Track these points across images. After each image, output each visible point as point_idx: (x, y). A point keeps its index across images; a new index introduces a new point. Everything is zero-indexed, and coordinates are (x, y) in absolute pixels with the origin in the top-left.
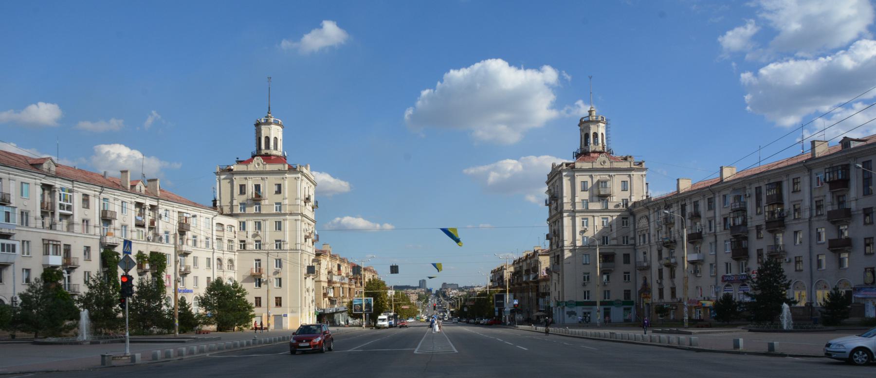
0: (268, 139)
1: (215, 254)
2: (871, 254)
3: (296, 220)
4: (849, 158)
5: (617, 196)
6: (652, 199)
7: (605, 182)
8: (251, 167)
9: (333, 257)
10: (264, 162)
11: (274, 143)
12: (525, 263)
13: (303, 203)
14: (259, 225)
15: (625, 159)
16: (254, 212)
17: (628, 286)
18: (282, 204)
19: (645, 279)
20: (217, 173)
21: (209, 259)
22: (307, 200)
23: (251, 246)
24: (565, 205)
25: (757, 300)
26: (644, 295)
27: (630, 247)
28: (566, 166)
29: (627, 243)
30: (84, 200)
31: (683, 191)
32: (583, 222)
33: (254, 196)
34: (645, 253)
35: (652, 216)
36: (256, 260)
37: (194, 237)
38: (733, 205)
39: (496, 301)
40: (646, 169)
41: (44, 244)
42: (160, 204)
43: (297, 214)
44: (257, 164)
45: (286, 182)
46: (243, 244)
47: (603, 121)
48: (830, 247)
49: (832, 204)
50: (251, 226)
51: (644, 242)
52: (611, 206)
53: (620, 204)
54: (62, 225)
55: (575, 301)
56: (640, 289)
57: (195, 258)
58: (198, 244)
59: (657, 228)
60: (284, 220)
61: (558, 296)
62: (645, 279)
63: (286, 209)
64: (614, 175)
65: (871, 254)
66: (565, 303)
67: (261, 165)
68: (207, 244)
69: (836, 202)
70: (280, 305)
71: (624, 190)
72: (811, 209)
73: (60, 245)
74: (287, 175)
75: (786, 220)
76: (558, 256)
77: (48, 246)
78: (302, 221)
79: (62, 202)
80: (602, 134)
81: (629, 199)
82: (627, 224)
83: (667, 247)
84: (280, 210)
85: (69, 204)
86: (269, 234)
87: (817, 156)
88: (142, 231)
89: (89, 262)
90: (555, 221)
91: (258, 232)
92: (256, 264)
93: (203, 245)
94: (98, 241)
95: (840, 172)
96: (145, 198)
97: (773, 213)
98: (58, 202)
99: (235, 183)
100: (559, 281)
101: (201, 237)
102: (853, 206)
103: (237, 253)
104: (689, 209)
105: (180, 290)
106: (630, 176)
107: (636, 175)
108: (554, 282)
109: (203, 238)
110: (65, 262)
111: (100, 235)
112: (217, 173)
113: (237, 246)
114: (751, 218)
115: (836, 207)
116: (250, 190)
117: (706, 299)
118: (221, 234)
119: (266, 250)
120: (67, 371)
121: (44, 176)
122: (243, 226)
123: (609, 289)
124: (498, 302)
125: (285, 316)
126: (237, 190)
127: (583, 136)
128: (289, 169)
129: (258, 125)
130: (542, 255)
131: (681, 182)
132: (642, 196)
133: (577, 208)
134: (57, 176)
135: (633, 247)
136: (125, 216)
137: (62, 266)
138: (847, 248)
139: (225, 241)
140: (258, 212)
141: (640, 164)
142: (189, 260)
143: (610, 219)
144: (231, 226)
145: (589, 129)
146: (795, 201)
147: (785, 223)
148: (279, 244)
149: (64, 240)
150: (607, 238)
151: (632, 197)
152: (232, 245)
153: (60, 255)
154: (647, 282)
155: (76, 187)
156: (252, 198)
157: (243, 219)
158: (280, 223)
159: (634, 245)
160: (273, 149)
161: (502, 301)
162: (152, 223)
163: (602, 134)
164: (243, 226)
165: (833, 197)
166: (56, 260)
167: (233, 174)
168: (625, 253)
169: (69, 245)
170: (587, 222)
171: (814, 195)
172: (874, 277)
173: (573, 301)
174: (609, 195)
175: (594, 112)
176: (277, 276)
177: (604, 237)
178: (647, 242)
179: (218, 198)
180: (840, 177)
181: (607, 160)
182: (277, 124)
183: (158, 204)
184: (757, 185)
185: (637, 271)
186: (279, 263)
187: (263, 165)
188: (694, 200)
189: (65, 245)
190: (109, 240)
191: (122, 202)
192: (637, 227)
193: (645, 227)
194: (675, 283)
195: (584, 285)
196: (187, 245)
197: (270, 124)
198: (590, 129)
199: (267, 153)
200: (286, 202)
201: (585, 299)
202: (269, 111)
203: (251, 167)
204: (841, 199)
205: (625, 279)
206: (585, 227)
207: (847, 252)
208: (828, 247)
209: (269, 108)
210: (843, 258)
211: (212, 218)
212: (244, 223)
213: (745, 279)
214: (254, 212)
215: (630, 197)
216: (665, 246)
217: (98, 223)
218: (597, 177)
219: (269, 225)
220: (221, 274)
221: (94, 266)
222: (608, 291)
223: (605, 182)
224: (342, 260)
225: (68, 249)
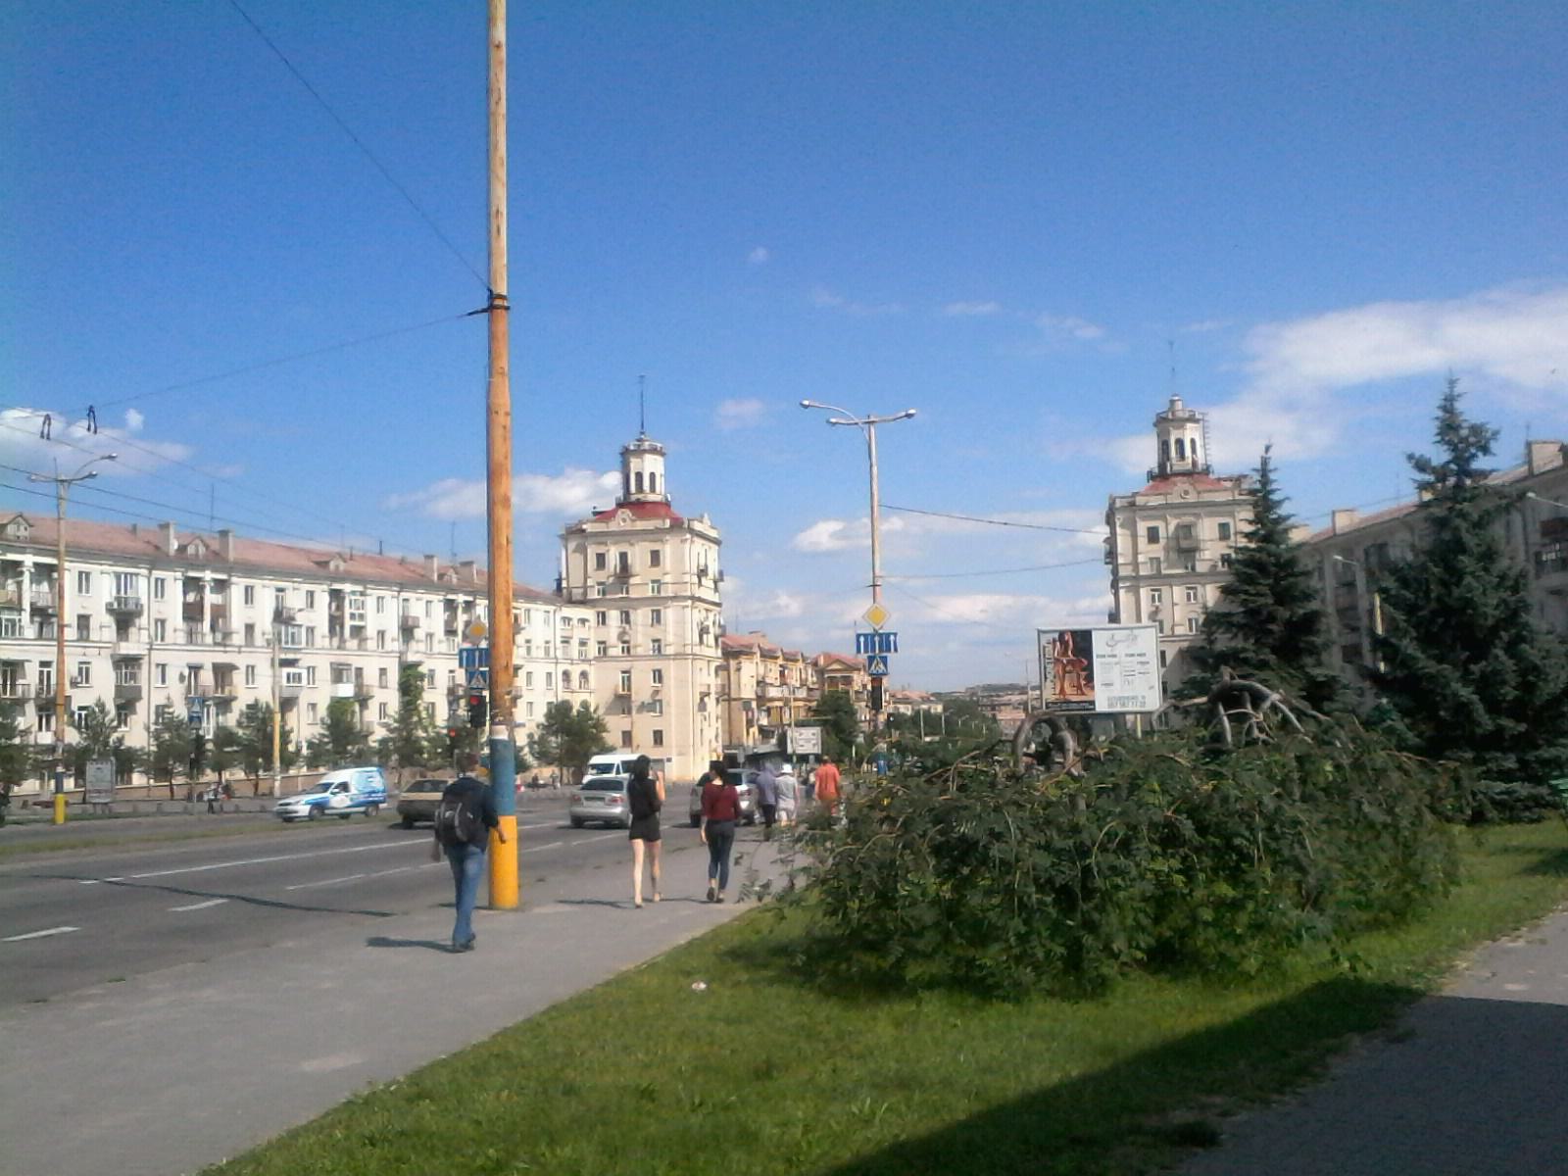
6: (604, 734)
8: (614, 526)
9: (768, 655)
13: (695, 579)
14: (626, 618)
22: (702, 573)
32: (1153, 596)
37: (528, 641)
43: (686, 598)
44: (624, 521)
50: (614, 616)
52: (1201, 567)
54: (352, 644)
57: (529, 674)
58: (534, 652)
68: (547, 651)
70: (661, 743)
77: (338, 673)
78: (692, 608)
79: (353, 611)
84: (659, 592)
85: (361, 611)
87: (1536, 472)
93: (541, 654)
98: (347, 611)
101: (538, 641)
113: (593, 650)
122: (602, 619)
125: (669, 760)
126: (592, 562)
128: (672, 526)
133: (1141, 573)
134: (343, 579)
139: (575, 643)
149: (356, 662)
153: (348, 681)
164: (602, 619)
166: (346, 690)
167: (586, 537)
170: (1160, 597)
175: (1180, 403)
179: (564, 575)
181: (1190, 488)
186: (658, 676)
190: (411, 658)
197: (645, 451)
200: (668, 579)
203: (614, 526)
206: (1157, 603)
212: (604, 614)
219: (641, 616)
220: (567, 696)
221: (392, 699)
224: (790, 658)
225: (359, 671)
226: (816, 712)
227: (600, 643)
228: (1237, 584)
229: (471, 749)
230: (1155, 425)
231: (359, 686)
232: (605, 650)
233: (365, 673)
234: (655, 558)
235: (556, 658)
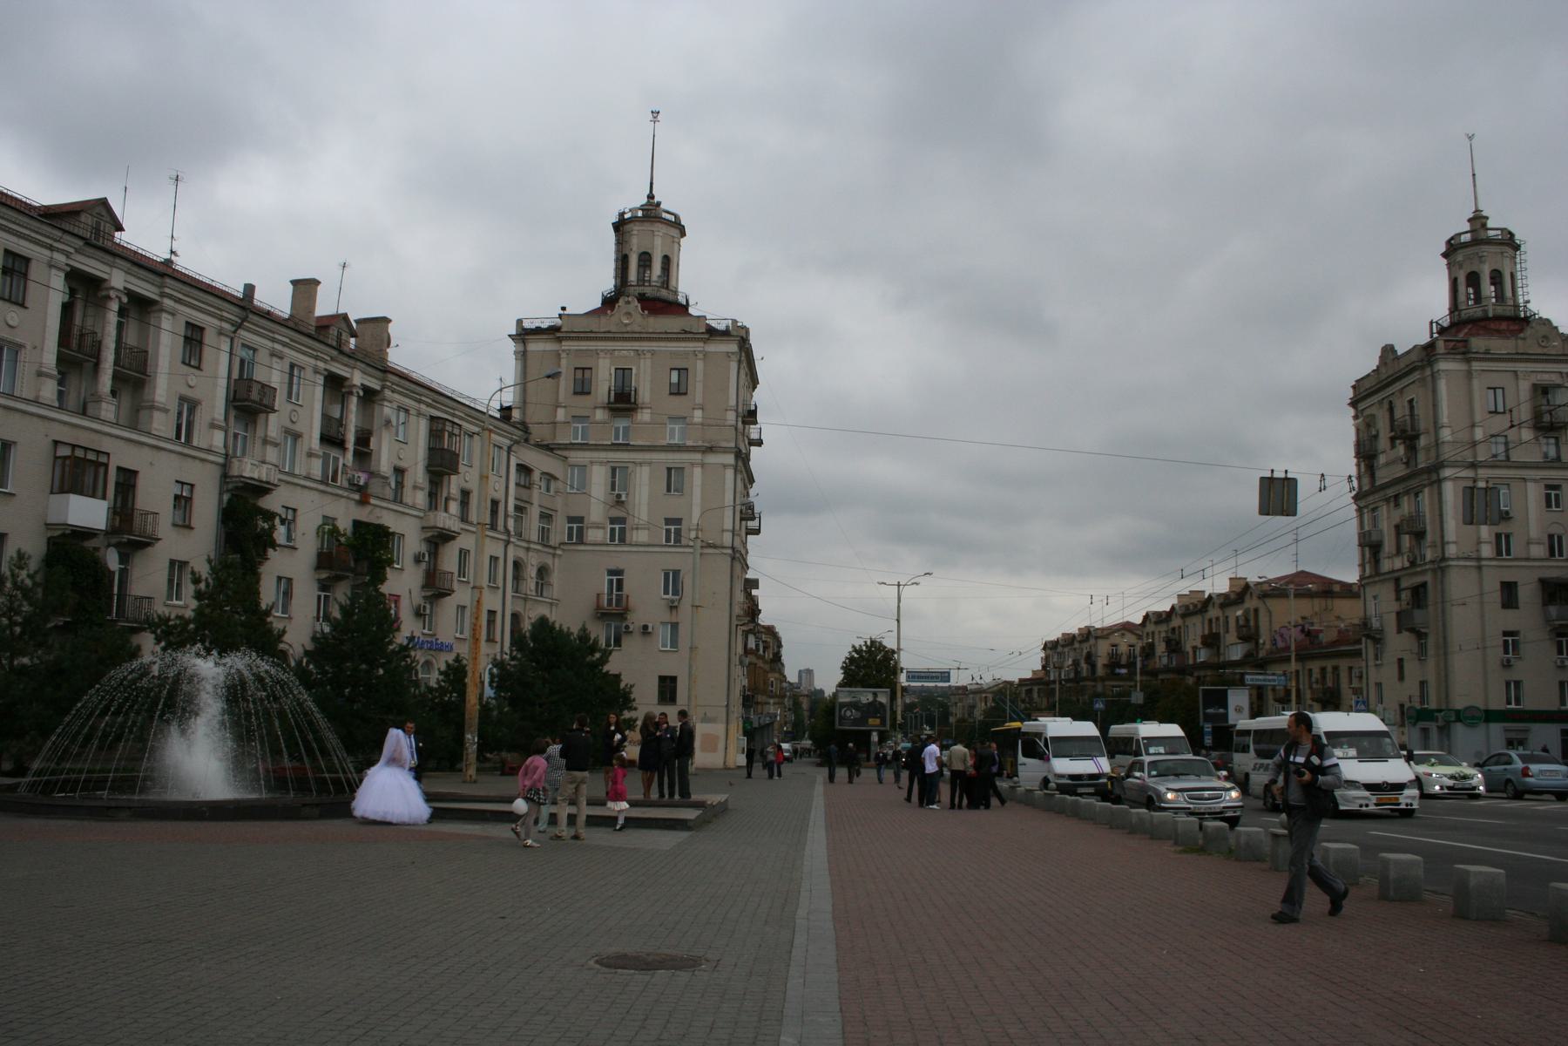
1: (511, 549)
12: (1163, 628)
21: (494, 559)
30: (187, 339)
33: (612, 399)
39: (1204, 708)
41: (56, 458)
42: (388, 388)
55: (1482, 707)
57: (463, 554)
66: (1453, 714)
73: (106, 466)
88: (336, 460)
89: (186, 531)
92: (611, 582)
94: (216, 472)
96: (352, 362)
105: (423, 642)
110: (117, 523)
111: (223, 451)
116: (604, 382)
118: (524, 493)
121: (81, 243)
123: (1517, 679)
124: (1209, 711)
136: (297, 408)
137: (107, 533)
149: (122, 456)
150: (1560, 538)
152: (548, 529)
153: (104, 498)
155: (170, 297)
156: (609, 403)
161: (1221, 711)
166: (89, 512)
169: (135, 473)
173: (1477, 708)
177: (1551, 537)
183: (383, 387)
186: (673, 580)
189: (119, 469)
190: (249, 469)
191: (292, 366)
195: (1507, 665)
196: (446, 510)
199: (644, 294)
201: (1509, 703)
211: (509, 450)
217: (222, 418)
222: (1518, 684)
225: (128, 480)
226: (177, 680)
228: (528, 634)
230: (1445, 255)
231: (124, 512)
232: (581, 531)
233: (142, 483)
235: (507, 532)
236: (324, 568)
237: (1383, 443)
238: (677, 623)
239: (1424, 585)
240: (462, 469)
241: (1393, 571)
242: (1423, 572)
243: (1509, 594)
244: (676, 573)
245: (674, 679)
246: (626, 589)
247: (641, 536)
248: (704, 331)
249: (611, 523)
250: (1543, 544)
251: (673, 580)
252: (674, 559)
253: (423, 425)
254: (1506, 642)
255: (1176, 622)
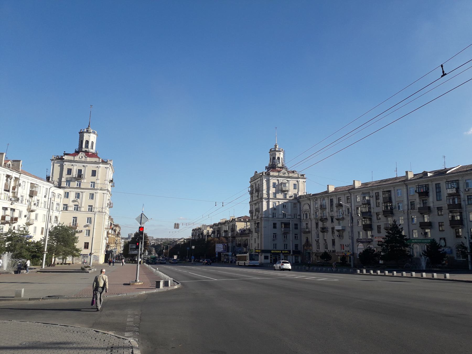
0: (87, 142)
2: (443, 231)
3: (104, 193)
4: (428, 181)
5: (292, 192)
7: (285, 184)
8: (77, 158)
10: (86, 156)
11: (91, 145)
12: (217, 227)
15: (293, 172)
16: (76, 186)
17: (297, 242)
18: (96, 183)
19: (307, 239)
20: (52, 160)
23: (71, 209)
24: (264, 195)
25: (193, 246)
26: (306, 247)
27: (298, 220)
28: (265, 174)
29: (296, 218)
31: (330, 192)
34: (307, 224)
35: (312, 203)
36: (74, 218)
38: (363, 201)
40: (305, 178)
43: (105, 190)
45: (100, 170)
46: (66, 207)
47: (282, 151)
48: (420, 226)
49: (420, 204)
51: (306, 217)
53: (293, 196)
56: (304, 244)
57: (37, 215)
59: (315, 211)
60: (95, 193)
61: (257, 246)
62: (307, 239)
63: (98, 186)
64: (290, 180)
65: (443, 231)
67: (84, 157)
69: (422, 203)
71: (295, 189)
72: (408, 205)
74: (101, 165)
75: (394, 211)
76: (258, 223)
80: (282, 158)
81: (297, 193)
82: (296, 208)
83: (322, 221)
86: (85, 201)
90: (256, 203)
91: (77, 200)
92: (74, 220)
93: (43, 205)
95: (424, 188)
97: (387, 207)
99: (65, 167)
100: (258, 237)
102: (431, 205)
103: (61, 212)
104: (335, 201)
106: (297, 181)
107: (301, 181)
108: (253, 238)
109: (43, 202)
112: (52, 160)
113: (61, 207)
114: (373, 209)
115: (422, 206)
116: (75, 173)
117: (347, 251)
119: (95, 212)
120: (121, 300)
122: (67, 195)
126: (65, 172)
127: (272, 158)
129: (81, 134)
130: (238, 222)
131: (329, 186)
132: (304, 193)
135: (299, 220)
138: (430, 227)
140: (78, 187)
141: (303, 175)
142: (33, 215)
143: (277, 204)
144: (60, 194)
145: (276, 155)
146: (398, 201)
147: (393, 212)
148: (91, 208)
151: (299, 193)
154: (308, 240)
157: (67, 190)
158: (93, 194)
159: (300, 219)
160: (90, 148)
162: (14, 188)
163: (282, 158)
164: (67, 195)
165: (420, 200)
168: (295, 223)
171: (409, 198)
172: (445, 243)
174: (287, 191)
176: (87, 228)
178: (308, 218)
179: (51, 176)
180: (424, 190)
182: (94, 133)
183: (20, 177)
184: (377, 191)
185: (302, 233)
187: (85, 157)
188: (338, 197)
192: (302, 209)
193: (307, 210)
194: (327, 241)
195: (274, 240)
197: (90, 133)
198: (276, 155)
201: (274, 248)
202: (89, 125)
204: (425, 202)
205: (295, 238)
207: (430, 229)
208: (419, 226)
209: (89, 123)
210: (427, 232)
212: (68, 193)
213: (371, 241)
214: (76, 186)
215: (298, 192)
216: (321, 221)
218: (281, 180)
219: (85, 196)
223: (285, 184)
227: (64, 205)
229: (380, 252)
234: (94, 173)
236: (3, 220)
237: (254, 192)
238: (90, 230)
239: (259, 223)
240: (38, 194)
241: (255, 219)
242: (259, 220)
243: (275, 226)
244: (91, 218)
245: (88, 243)
246: (77, 222)
247: (83, 209)
248: (101, 162)
249: (75, 206)
250: (282, 215)
251: (89, 220)
252: (90, 215)
253: (29, 185)
254: (274, 236)
255: (220, 226)
